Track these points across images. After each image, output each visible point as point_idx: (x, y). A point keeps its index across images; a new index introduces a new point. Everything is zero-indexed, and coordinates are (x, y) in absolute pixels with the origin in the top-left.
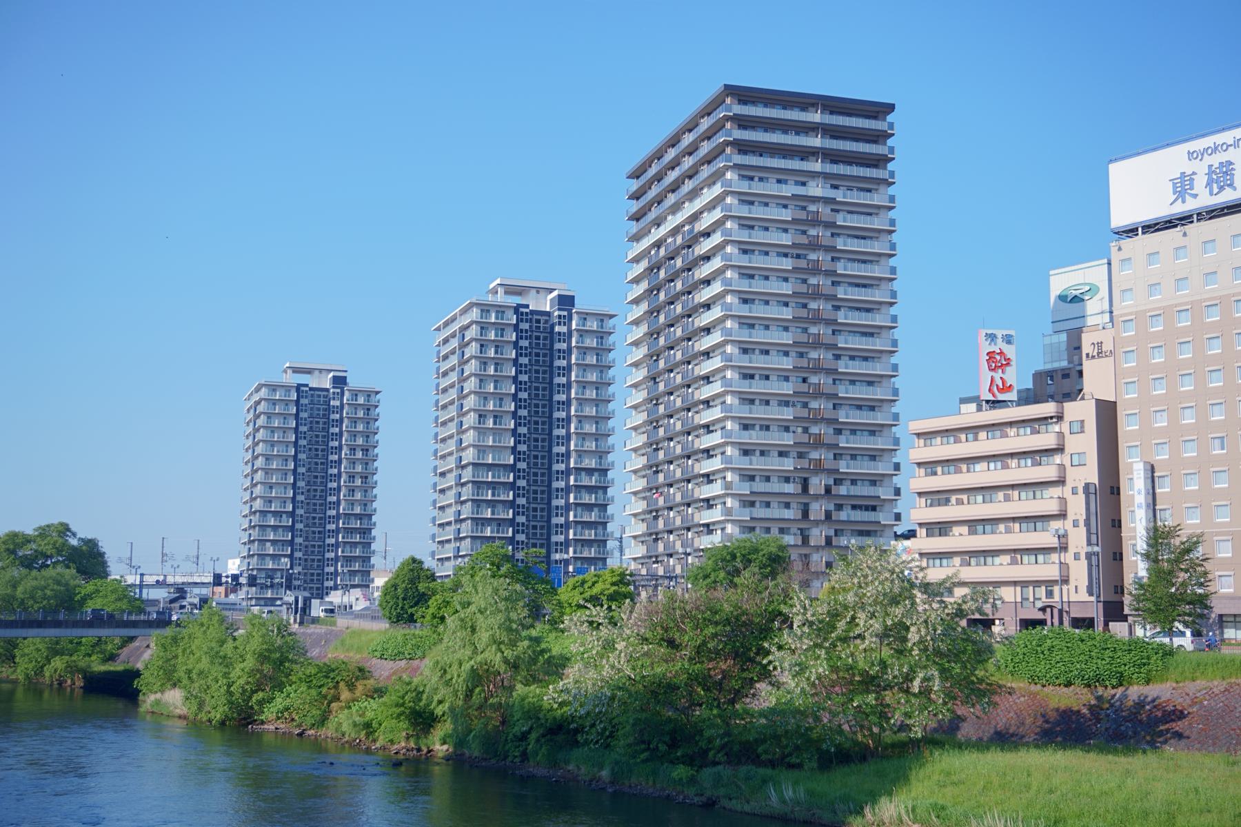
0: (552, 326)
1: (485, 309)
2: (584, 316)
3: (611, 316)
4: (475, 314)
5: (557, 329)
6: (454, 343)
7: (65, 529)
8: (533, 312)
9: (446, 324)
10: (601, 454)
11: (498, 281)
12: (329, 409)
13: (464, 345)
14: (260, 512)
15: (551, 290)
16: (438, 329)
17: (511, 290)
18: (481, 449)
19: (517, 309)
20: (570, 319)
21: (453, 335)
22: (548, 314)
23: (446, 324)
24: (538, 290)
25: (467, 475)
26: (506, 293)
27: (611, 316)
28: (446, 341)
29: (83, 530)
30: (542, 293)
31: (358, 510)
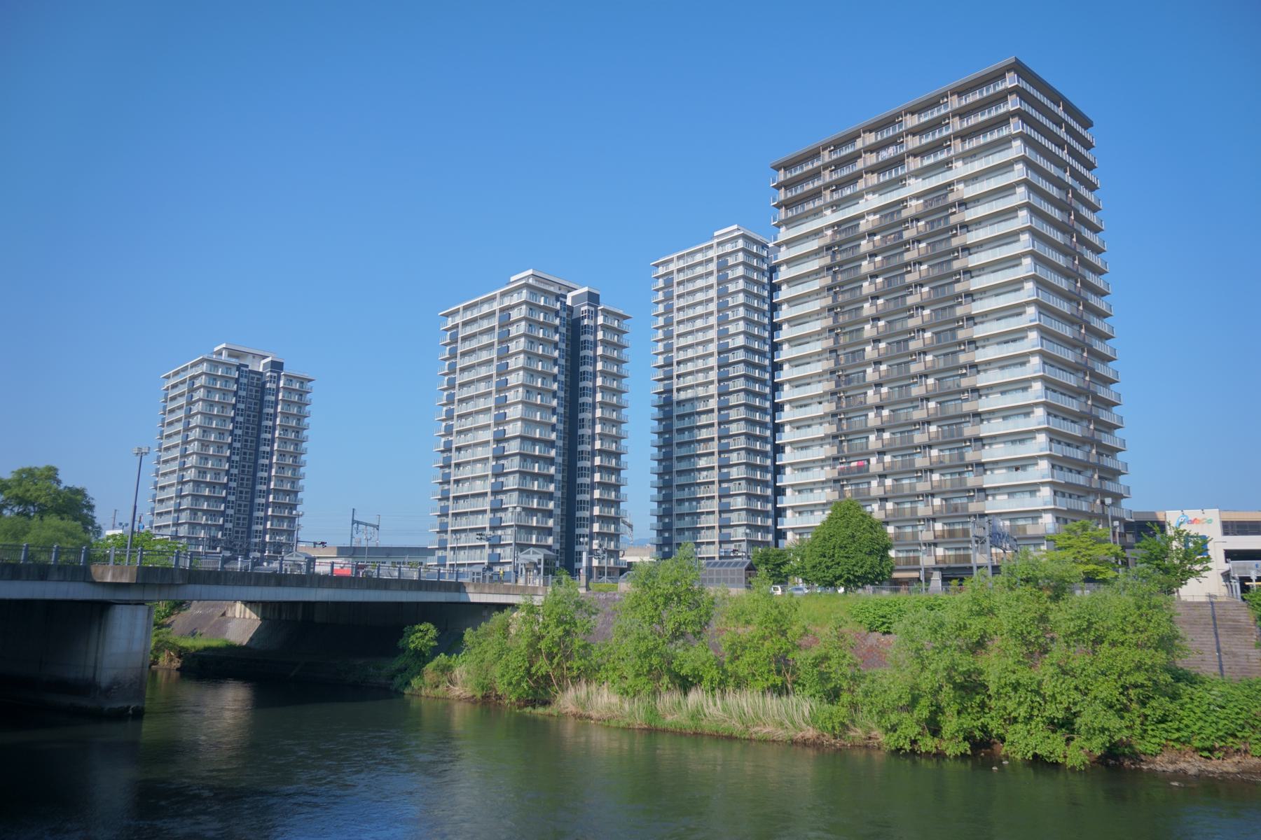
0: (264, 383)
1: (215, 364)
2: (290, 378)
3: (310, 380)
4: (204, 367)
5: (268, 385)
6: (184, 388)
7: (51, 474)
8: (251, 372)
9: (176, 373)
10: (294, 481)
11: (224, 345)
12: (262, 389)
13: (192, 390)
14: (194, 481)
15: (265, 357)
16: (168, 377)
17: (233, 353)
18: (202, 472)
19: (238, 368)
20: (279, 379)
21: (183, 382)
22: (261, 374)
23: (176, 373)
24: (254, 355)
25: (187, 489)
26: (229, 356)
27: (310, 380)
28: (174, 386)
29: (68, 479)
30: (257, 359)
31: (288, 487)
